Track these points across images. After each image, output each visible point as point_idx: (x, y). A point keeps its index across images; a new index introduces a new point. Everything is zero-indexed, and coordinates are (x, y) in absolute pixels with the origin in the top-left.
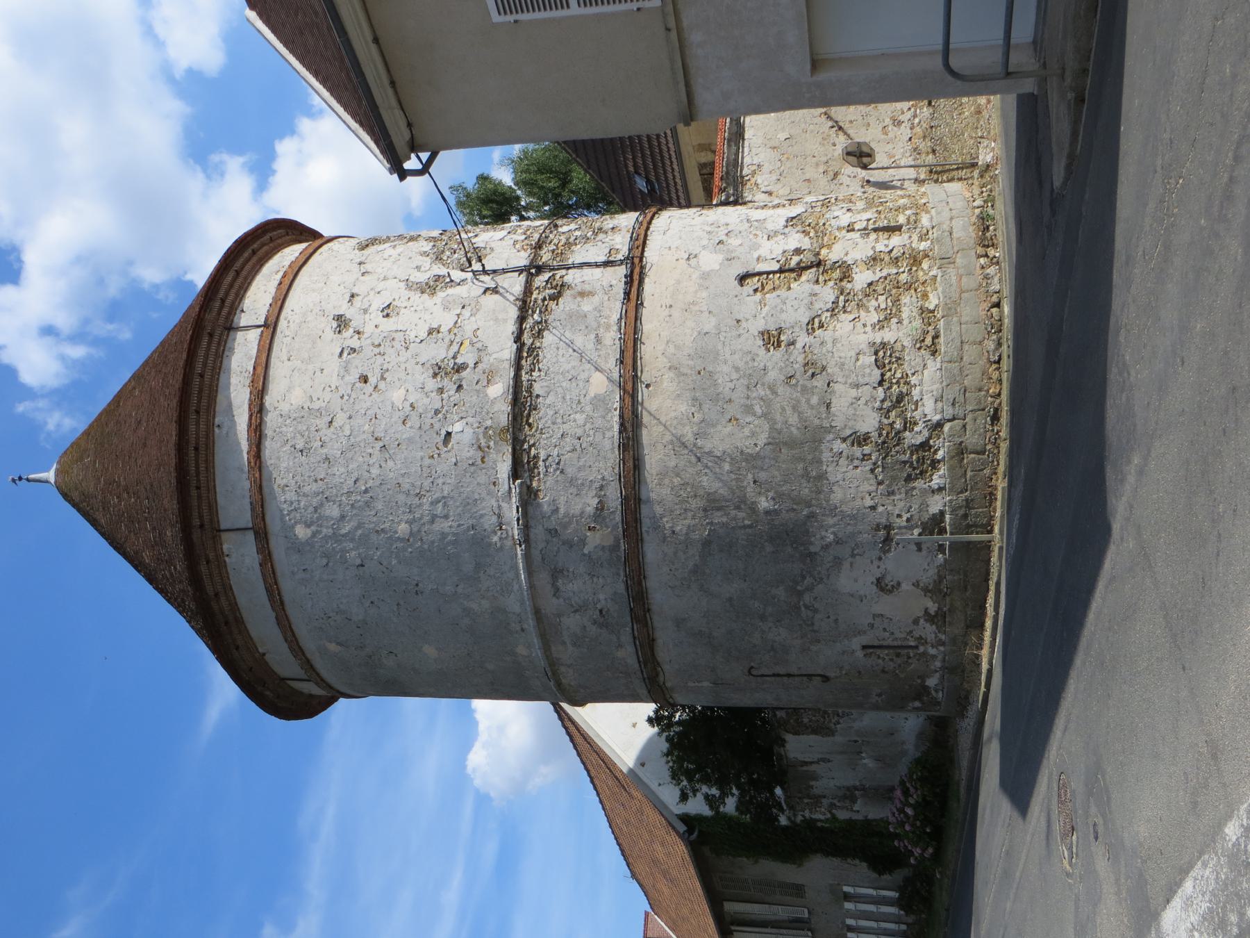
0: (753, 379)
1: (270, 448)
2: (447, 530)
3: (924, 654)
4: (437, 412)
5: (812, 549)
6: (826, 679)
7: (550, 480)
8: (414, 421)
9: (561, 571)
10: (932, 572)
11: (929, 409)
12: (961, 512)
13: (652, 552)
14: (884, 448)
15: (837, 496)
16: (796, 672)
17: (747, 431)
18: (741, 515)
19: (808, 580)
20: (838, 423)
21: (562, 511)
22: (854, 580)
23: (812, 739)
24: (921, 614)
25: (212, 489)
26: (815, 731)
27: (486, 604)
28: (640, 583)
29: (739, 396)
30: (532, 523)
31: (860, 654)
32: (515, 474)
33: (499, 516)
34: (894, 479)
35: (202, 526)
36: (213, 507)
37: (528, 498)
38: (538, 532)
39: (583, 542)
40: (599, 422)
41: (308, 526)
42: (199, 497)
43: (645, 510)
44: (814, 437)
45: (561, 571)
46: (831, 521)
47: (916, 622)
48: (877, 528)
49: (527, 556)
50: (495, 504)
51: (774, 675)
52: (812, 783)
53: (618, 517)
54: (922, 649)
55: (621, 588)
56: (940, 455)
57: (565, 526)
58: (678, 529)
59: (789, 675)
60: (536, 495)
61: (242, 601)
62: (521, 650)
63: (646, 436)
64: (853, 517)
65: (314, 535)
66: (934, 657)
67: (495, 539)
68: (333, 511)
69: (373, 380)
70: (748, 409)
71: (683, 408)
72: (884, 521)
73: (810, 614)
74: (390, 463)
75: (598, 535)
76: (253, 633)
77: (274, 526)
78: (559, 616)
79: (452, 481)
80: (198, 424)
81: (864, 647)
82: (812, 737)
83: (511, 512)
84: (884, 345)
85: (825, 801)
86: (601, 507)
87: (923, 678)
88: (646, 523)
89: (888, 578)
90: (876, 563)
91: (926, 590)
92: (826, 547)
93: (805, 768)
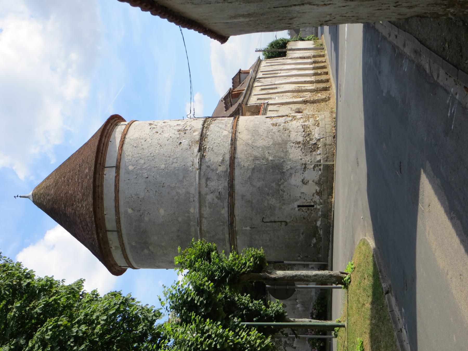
0: (268, 132)
1: (125, 147)
2: (176, 166)
3: (316, 208)
4: (178, 138)
5: (284, 171)
6: (286, 224)
7: (209, 153)
8: (171, 139)
9: (209, 179)
10: (318, 177)
11: (317, 136)
12: (326, 159)
13: (237, 172)
14: (304, 144)
15: (291, 156)
16: (277, 220)
17: (267, 142)
18: (264, 161)
19: (282, 181)
20: (292, 139)
21: (212, 161)
22: (295, 180)
24: (315, 192)
25: (105, 155)
27: (184, 190)
28: (232, 182)
29: (265, 134)
30: (202, 164)
31: (297, 209)
32: (200, 150)
33: (193, 162)
34: (307, 152)
35: (100, 164)
36: (104, 160)
37: (202, 157)
38: (204, 167)
39: (217, 169)
40: (225, 140)
41: (133, 166)
42: (101, 156)
43: (236, 160)
44: (285, 143)
45: (209, 179)
46: (289, 163)
47: (313, 195)
48: (302, 164)
49: (200, 174)
50: (192, 159)
51: (270, 222)
53: (228, 163)
54: (315, 206)
55: (226, 184)
56: (319, 146)
57: (212, 165)
58: (245, 165)
59: (275, 222)
60: (204, 157)
61: (105, 191)
62: (192, 210)
63: (238, 143)
64: (295, 161)
65: (135, 168)
66: (319, 209)
67: (191, 169)
68: (142, 162)
69: (159, 132)
70: (267, 137)
71: (249, 137)
72: (304, 162)
73: (282, 193)
74: (162, 149)
75: (221, 167)
76: (105, 205)
77: (122, 165)
78: (206, 194)
79: (180, 153)
80: (105, 139)
81: (299, 206)
83: (197, 161)
84: (305, 125)
86: (223, 160)
88: (236, 164)
89: (305, 179)
90: (302, 175)
91: (316, 183)
92: (288, 170)
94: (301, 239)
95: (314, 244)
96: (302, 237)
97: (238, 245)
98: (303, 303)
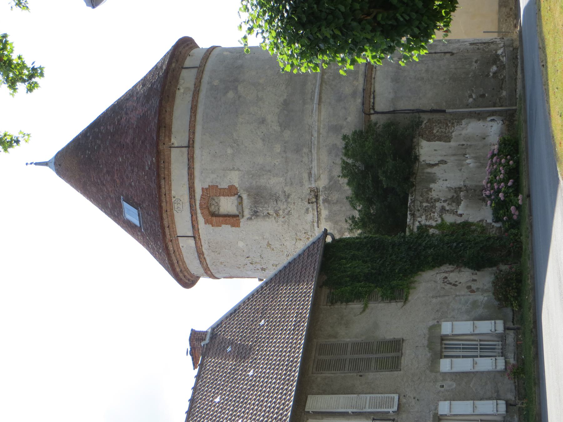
6: (452, 54)
23: (437, 144)
26: (440, 139)
52: (432, 186)
59: (435, 53)
82: (438, 143)
85: (438, 205)
87: (496, 50)
93: (429, 170)
94: (474, 67)
95: (495, 73)
96: (475, 66)
97: (377, 79)
98: (476, 158)
